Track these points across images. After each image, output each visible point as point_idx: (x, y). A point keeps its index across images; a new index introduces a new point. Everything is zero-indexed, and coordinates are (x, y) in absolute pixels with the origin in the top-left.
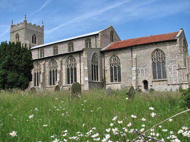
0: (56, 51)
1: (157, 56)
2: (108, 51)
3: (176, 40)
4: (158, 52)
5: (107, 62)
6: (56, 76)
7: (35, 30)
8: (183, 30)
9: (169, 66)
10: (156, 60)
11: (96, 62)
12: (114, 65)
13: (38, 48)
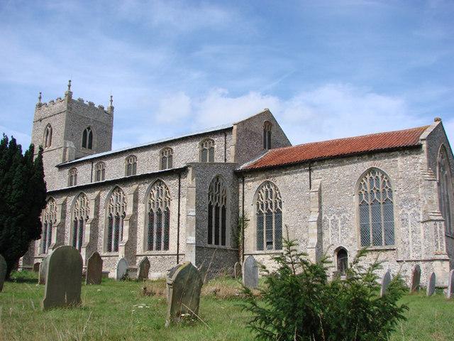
0: (166, 158)
1: (372, 186)
2: (253, 172)
3: (419, 147)
4: (374, 178)
5: (250, 195)
6: (51, 233)
8: (441, 123)
9: (400, 212)
10: (369, 196)
11: (221, 199)
12: (267, 207)
13: (92, 161)
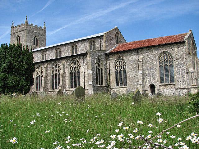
0: (58, 53)
1: (164, 59)
2: (113, 54)
3: (184, 42)
4: (165, 55)
5: (112, 65)
6: (59, 80)
7: (37, 31)
8: (192, 32)
9: (177, 69)
10: (163, 63)
11: (100, 65)
12: (120, 68)
13: (40, 51)
